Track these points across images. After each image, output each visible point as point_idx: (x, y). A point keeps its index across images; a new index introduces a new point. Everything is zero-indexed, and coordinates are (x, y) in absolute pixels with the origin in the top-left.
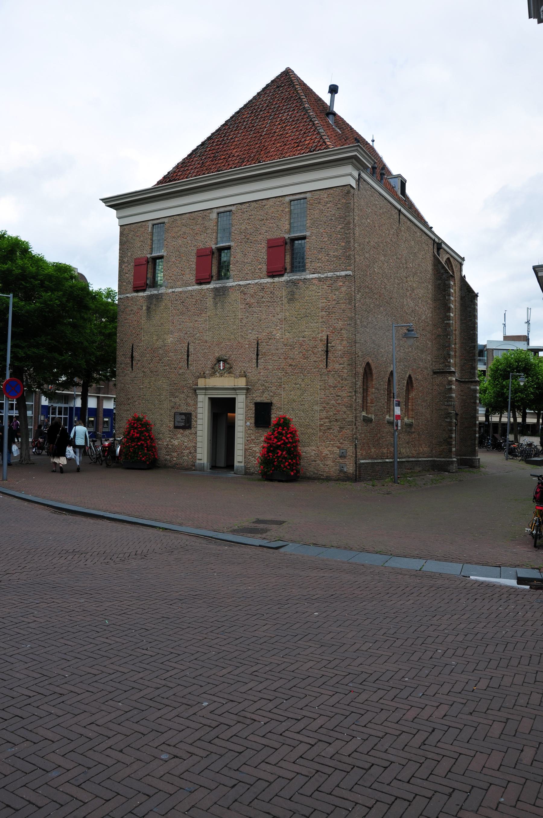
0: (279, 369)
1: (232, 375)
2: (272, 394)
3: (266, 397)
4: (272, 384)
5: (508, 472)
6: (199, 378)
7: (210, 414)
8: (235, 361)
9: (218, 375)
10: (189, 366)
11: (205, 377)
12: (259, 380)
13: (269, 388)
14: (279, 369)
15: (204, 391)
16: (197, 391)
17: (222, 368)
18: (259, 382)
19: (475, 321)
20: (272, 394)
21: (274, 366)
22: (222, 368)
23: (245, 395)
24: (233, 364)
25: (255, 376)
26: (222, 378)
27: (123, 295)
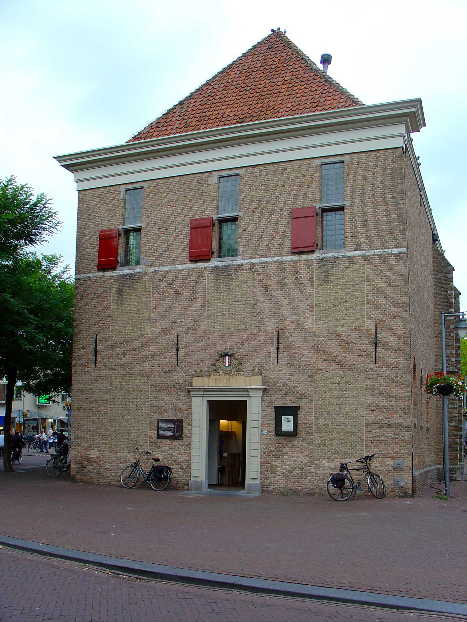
0: (309, 365)
1: (242, 373)
3: (290, 400)
6: (193, 376)
8: (245, 355)
9: (221, 373)
10: (179, 362)
14: (309, 365)
17: (227, 365)
22: (227, 365)
25: (274, 374)
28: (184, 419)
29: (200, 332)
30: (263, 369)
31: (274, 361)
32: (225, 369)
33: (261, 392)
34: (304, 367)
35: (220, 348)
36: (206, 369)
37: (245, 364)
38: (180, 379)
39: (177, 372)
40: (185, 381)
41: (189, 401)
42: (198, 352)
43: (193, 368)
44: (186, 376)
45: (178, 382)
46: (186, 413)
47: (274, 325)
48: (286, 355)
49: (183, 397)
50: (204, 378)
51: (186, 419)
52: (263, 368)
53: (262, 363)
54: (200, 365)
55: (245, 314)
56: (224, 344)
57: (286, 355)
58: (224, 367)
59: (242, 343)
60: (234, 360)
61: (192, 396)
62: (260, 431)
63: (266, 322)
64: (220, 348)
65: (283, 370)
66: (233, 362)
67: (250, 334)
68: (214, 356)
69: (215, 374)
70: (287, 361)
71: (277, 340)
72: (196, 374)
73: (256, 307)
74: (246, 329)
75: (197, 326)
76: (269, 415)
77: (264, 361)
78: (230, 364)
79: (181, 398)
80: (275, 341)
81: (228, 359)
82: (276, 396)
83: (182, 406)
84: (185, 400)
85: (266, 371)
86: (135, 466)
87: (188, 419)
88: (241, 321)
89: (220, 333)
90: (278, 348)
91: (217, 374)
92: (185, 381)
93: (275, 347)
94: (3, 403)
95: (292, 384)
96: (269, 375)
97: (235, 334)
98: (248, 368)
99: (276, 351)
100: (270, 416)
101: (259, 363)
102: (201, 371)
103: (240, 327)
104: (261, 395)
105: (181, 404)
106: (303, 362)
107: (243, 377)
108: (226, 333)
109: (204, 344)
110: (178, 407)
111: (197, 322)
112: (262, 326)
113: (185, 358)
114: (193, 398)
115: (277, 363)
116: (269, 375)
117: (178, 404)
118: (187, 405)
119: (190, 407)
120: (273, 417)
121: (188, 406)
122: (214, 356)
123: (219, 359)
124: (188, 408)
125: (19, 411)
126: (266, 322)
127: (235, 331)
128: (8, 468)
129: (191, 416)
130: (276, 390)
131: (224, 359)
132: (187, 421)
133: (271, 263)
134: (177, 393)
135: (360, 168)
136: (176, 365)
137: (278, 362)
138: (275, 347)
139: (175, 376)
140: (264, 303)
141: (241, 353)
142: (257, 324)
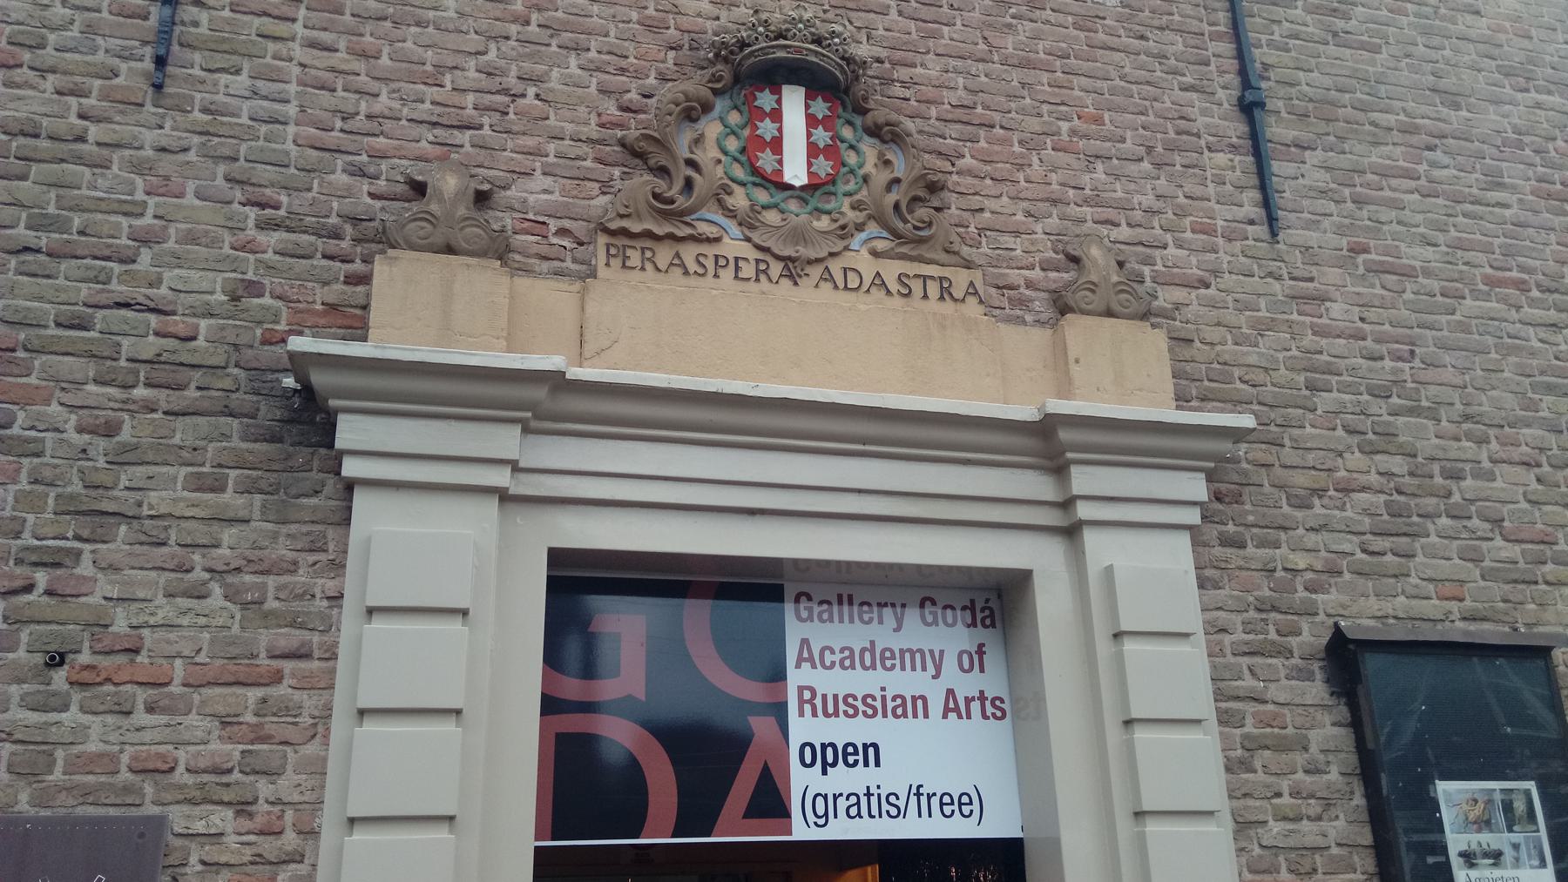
0: (1521, 286)
1: (961, 279)
2: (1500, 549)
3: (1452, 589)
4: (1482, 441)
5: (1225, 364)
6: (384, 240)
7: (550, 797)
8: (963, 115)
9: (734, 246)
10: (190, 65)
11: (499, 251)
12: (1318, 376)
13: (1457, 476)
14: (1521, 286)
15: (505, 441)
16: (350, 432)
17: (796, 171)
18: (1324, 401)
19: (1368, 801)
20: (1500, 549)
21: (1458, 246)
22: (796, 171)
23: (1184, 541)
24: (951, 157)
25: (1262, 327)
26: (811, 295)
27: (1207, 258)
28: (178, 817)
30: (1146, 270)
31: (1241, 213)
32: (772, 217)
33: (1195, 487)
34: (1487, 297)
36: (537, 192)
37: (975, 202)
38: (178, 260)
39: (138, 168)
40: (254, 288)
41: (283, 550)
44: (264, 225)
45: (140, 293)
46: (226, 722)
48: (1320, 178)
49: (200, 484)
50: (523, 283)
51: (222, 819)
53: (1138, 215)
54: (465, 137)
57: (1320, 178)
58: (762, 196)
60: (869, 148)
61: (351, 468)
62: (342, 652)
65: (1323, 299)
66: (852, 159)
68: (639, 75)
69: (664, 255)
70: (1340, 231)
71: (1227, 48)
72: (431, 219)
76: (1281, 746)
77: (1148, 200)
79: (158, 500)
80: (1214, 47)
81: (812, 121)
82: (1312, 539)
83: (165, 610)
84: (228, 535)
85: (1179, 294)
86: (743, 44)
87: (243, 808)
90: (1249, 108)
91: (689, 253)
92: (254, 288)
93: (1221, 94)
95: (1426, 437)
96: (1213, 334)
98: (1008, 241)
99: (1236, 129)
100: (1299, 759)
101: (1110, 214)
104: (1193, 517)
105: (146, 583)
106: (1470, 256)
107: (972, 308)
110: (100, 625)
113: (282, 29)
114: (360, 499)
115: (1261, 230)
116: (1213, 334)
117: (106, 587)
118: (252, 606)
119: (289, 638)
120: (1334, 775)
121: (270, 619)
124: (265, 638)
128: (60, 627)
129: (318, 769)
130: (1300, 479)
131: (760, 114)
132: (232, 848)
134: (110, 430)
136: (133, 74)
137: (1272, 220)
138: (1227, 96)
139: (98, 206)
141: (929, 92)
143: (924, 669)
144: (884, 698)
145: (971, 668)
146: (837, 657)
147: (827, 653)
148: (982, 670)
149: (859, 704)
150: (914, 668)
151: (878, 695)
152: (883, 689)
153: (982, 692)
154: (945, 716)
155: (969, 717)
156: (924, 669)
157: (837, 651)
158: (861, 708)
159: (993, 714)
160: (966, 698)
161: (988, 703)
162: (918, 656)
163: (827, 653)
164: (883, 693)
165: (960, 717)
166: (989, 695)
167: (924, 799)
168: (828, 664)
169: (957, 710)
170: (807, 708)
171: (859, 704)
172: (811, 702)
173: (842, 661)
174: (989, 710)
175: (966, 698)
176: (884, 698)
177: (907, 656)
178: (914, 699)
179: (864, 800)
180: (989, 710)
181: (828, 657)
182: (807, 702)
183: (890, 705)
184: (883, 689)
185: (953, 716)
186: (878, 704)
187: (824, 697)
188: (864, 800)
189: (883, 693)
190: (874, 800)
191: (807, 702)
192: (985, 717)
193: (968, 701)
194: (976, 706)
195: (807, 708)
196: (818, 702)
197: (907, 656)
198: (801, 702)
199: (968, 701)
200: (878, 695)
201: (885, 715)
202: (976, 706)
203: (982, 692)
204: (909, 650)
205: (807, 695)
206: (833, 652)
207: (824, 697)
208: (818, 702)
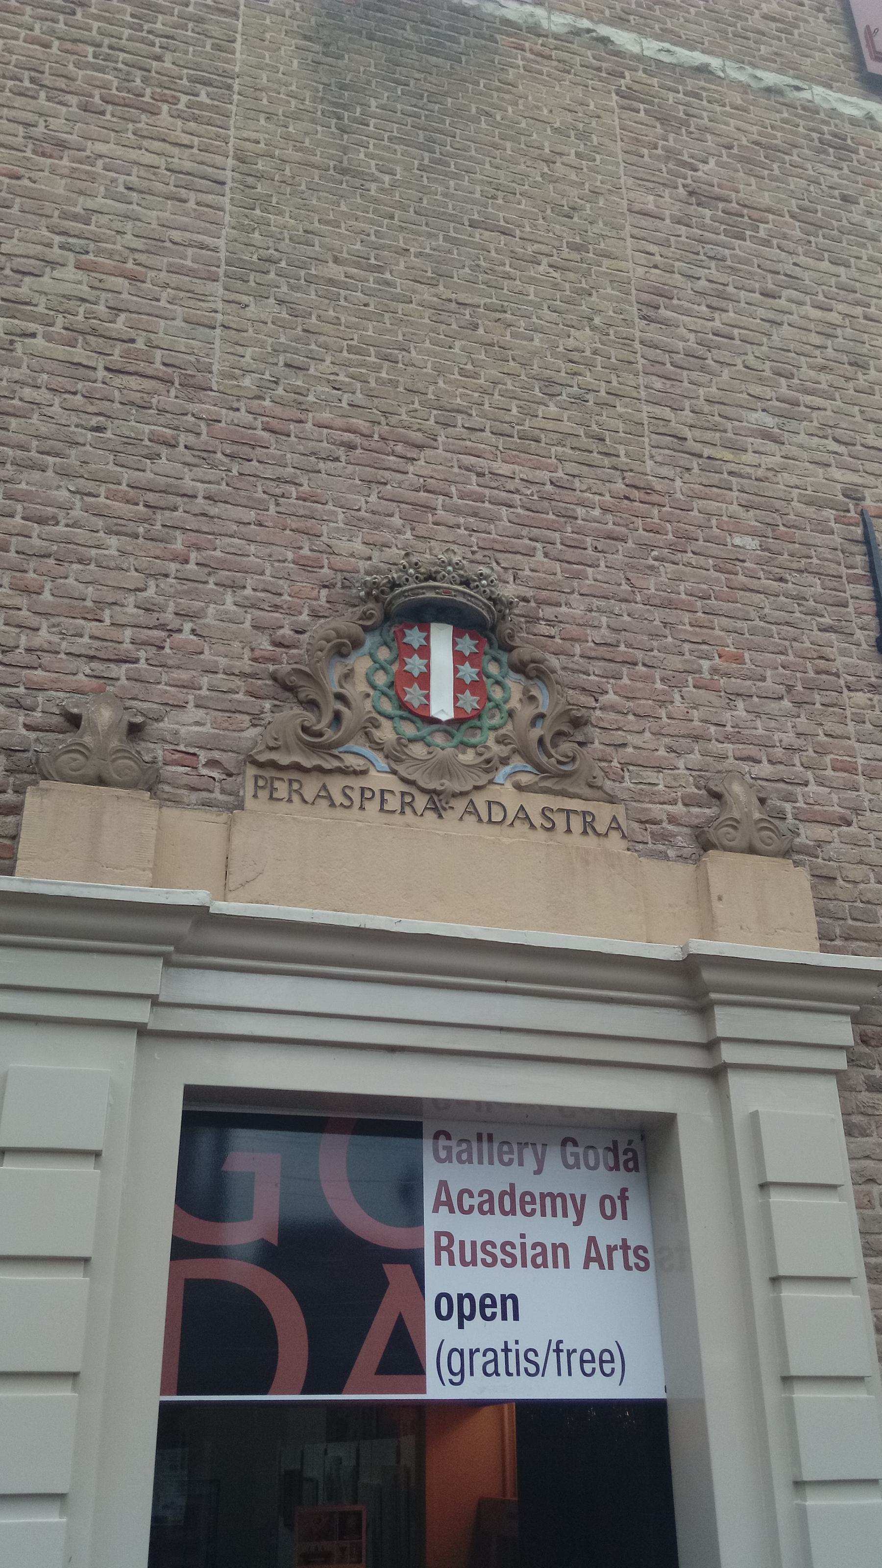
1: (604, 813)
29: (142, 367)
30: (788, 807)
32: (418, 750)
35: (357, 546)
42: (113, 541)
43: (35, 688)
47: (820, 471)
50: (171, 814)
52: (790, 798)
53: (779, 752)
55: (584, 338)
56: (396, 521)
58: (409, 730)
59: (570, 555)
63: (753, 433)
64: (357, 546)
66: (497, 694)
67: (635, 494)
69: (311, 787)
72: (84, 751)
73: (663, 312)
74: (594, 445)
75: (116, 310)
77: (789, 738)
78: (470, 701)
80: (852, 589)
85: (821, 832)
88: (550, 382)
89: (360, 423)
91: (336, 785)
93: (859, 635)
94: (716, 991)
96: (856, 872)
97: (505, 469)
98: (650, 776)
102: (135, 731)
103: (540, 423)
108: (417, 437)
109: (188, 484)
111: (120, 283)
112: (728, 455)
122: (292, 611)
123: (357, 644)
125: (12, 832)
126: (753, 433)
127: (501, 442)
131: (410, 650)
133: (745, 88)
135: (549, 58)
140: (723, 304)
141: (573, 630)
142: (687, 433)
143: (565, 1215)
144: (523, 1245)
145: (613, 1215)
146: (476, 1201)
147: (466, 1196)
148: (625, 1217)
149: (498, 1252)
150: (554, 1214)
151: (517, 1242)
152: (523, 1236)
153: (624, 1241)
154: (586, 1266)
155: (611, 1267)
156: (565, 1215)
157: (476, 1195)
158: (500, 1256)
159: (637, 1265)
160: (608, 1247)
161: (631, 1253)
162: (559, 1201)
163: (466, 1196)
164: (523, 1240)
165: (602, 1267)
166: (632, 1243)
167: (564, 1356)
168: (466, 1208)
169: (598, 1259)
170: (444, 1255)
171: (498, 1252)
172: (448, 1249)
173: (481, 1205)
174: (632, 1260)
175: (608, 1247)
176: (523, 1245)
177: (548, 1200)
178: (555, 1247)
179: (501, 1356)
180: (632, 1260)
181: (467, 1202)
182: (444, 1249)
183: (530, 1253)
184: (523, 1236)
185: (594, 1266)
186: (517, 1252)
187: (462, 1243)
188: (501, 1356)
189: (523, 1240)
190: (512, 1356)
191: (444, 1249)
192: (628, 1267)
193: (611, 1249)
194: (618, 1255)
195: (444, 1255)
196: (456, 1249)
197: (548, 1200)
198: (438, 1249)
199: (611, 1249)
200: (517, 1242)
201: (524, 1265)
202: (618, 1255)
203: (624, 1241)
204: (550, 1194)
205: (444, 1241)
206: (471, 1196)
207: (462, 1243)
208: (456, 1249)
